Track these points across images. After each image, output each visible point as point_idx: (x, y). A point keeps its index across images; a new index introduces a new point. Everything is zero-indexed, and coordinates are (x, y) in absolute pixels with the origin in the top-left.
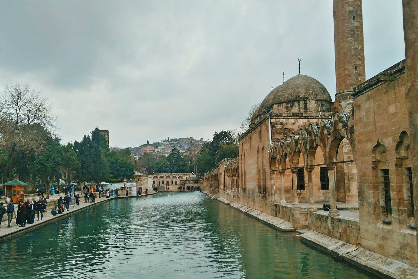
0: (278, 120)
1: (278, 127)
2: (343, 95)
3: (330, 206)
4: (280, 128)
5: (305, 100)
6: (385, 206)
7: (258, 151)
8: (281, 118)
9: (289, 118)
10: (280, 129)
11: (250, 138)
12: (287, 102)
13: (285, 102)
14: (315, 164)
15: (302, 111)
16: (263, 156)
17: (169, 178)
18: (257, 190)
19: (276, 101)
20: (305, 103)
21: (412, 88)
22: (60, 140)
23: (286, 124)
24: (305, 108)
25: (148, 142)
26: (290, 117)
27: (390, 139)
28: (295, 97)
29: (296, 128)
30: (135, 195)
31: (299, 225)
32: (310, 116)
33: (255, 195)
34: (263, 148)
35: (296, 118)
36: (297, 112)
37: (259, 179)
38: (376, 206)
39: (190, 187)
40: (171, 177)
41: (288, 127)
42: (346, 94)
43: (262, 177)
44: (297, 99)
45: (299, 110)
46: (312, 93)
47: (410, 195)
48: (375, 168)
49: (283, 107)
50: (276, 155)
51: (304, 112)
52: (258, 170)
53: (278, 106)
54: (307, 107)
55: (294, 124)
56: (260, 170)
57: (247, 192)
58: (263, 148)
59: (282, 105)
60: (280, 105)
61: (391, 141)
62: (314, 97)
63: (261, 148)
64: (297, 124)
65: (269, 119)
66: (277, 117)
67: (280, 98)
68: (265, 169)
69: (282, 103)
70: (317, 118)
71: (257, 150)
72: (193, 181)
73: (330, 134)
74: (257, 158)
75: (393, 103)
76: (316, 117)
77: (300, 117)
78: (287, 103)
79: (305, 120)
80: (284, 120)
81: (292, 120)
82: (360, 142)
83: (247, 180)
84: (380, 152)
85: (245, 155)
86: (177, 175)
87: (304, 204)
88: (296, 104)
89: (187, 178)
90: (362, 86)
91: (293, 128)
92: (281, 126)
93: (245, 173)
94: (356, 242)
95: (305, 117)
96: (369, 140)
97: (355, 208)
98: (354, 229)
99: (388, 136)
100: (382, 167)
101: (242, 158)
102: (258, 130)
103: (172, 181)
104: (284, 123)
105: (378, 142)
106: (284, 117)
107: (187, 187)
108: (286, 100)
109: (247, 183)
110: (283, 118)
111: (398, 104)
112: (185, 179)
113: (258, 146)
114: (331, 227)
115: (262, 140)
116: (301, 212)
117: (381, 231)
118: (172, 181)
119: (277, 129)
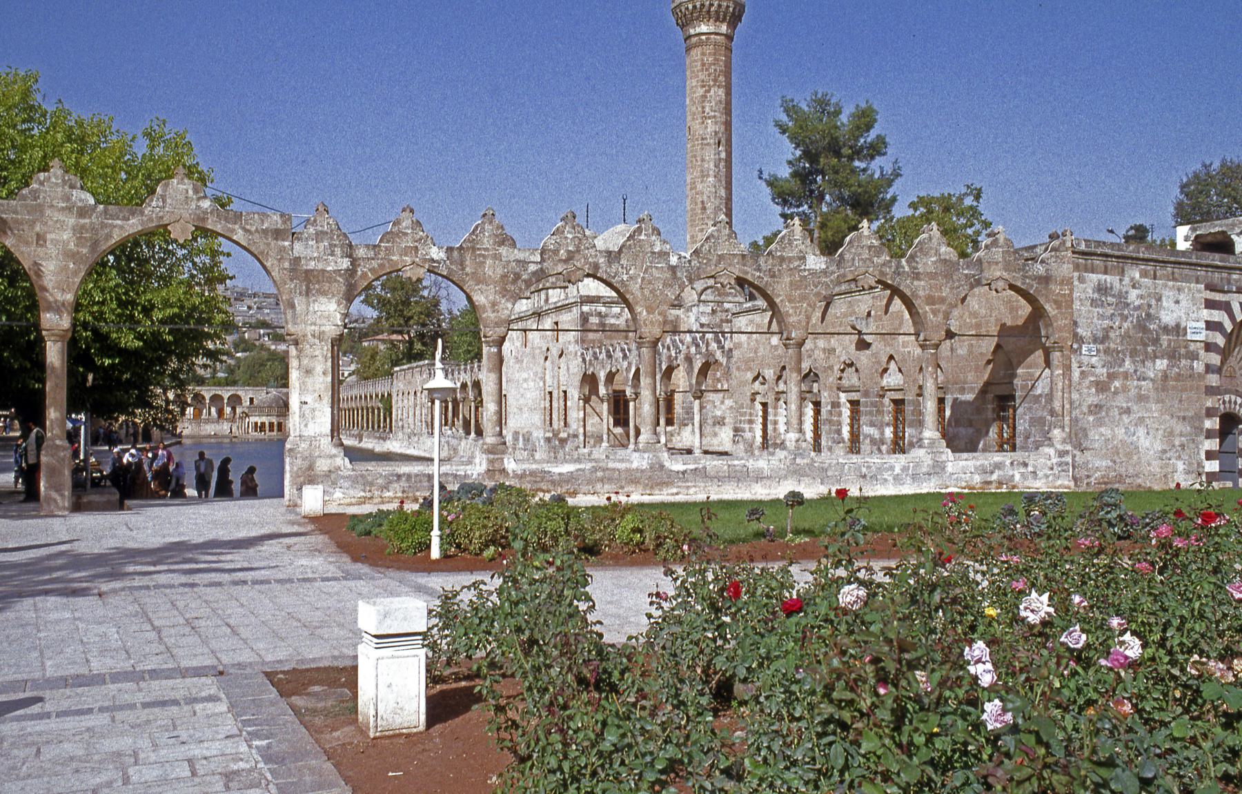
1: (594, 320)
23: (606, 315)
63: (555, 352)
73: (700, 353)
80: (603, 309)
89: (251, 400)
96: (750, 369)
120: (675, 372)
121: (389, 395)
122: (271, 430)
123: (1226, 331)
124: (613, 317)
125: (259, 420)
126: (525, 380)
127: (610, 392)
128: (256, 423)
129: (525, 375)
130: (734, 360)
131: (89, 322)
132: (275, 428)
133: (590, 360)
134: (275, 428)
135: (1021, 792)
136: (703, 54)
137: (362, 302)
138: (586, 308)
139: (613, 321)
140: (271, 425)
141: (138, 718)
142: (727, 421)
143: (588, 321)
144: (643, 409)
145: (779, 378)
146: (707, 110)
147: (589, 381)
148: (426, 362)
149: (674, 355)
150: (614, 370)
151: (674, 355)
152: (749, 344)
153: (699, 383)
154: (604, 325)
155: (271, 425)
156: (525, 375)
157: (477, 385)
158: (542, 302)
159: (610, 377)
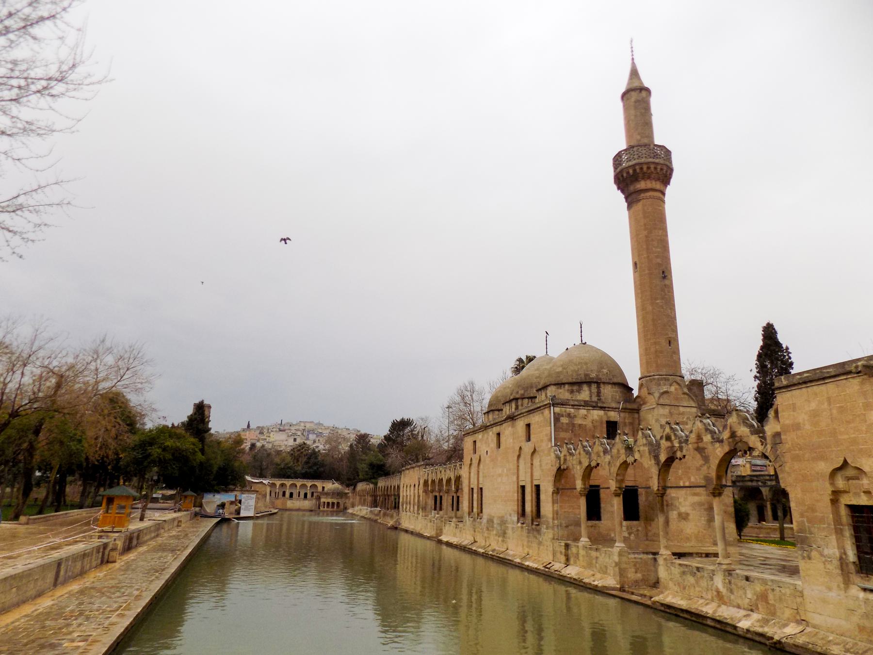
0: (563, 409)
1: (564, 420)
2: (654, 379)
5: (598, 384)
6: (858, 563)
8: (568, 407)
9: (579, 407)
12: (571, 384)
14: (669, 485)
15: (595, 399)
17: (294, 487)
18: (515, 519)
19: (553, 380)
20: (598, 387)
22: (144, 415)
23: (575, 416)
24: (599, 394)
26: (581, 406)
28: (583, 376)
29: (588, 423)
30: (253, 515)
31: (626, 579)
32: (608, 408)
33: (507, 527)
35: (589, 408)
36: (587, 399)
38: (842, 561)
39: (328, 503)
40: (298, 486)
41: (578, 421)
42: (658, 379)
44: (586, 379)
45: (591, 397)
46: (607, 373)
48: (834, 501)
49: (565, 390)
50: (573, 465)
51: (598, 399)
52: (518, 487)
53: (558, 388)
54: (600, 393)
55: (585, 417)
57: (484, 521)
59: (564, 387)
60: (561, 386)
62: (611, 379)
64: (590, 418)
65: (552, 408)
66: (562, 405)
67: (559, 377)
69: (564, 384)
70: (617, 410)
72: (333, 493)
74: (516, 467)
76: (616, 408)
77: (594, 407)
78: (559, 386)
79: (601, 413)
80: (572, 410)
81: (583, 412)
84: (847, 477)
86: (309, 483)
87: (711, 552)
88: (585, 388)
89: (323, 488)
90: (798, 377)
91: (584, 423)
94: (795, 617)
95: (602, 408)
97: (701, 553)
98: (788, 595)
100: (851, 501)
103: (299, 492)
104: (572, 415)
106: (572, 405)
107: (324, 502)
108: (570, 380)
110: (570, 407)
112: (320, 489)
114: (724, 587)
116: (629, 559)
117: (862, 604)
118: (299, 492)
119: (562, 423)
121: (399, 487)
122: (333, 507)
125: (326, 500)
126: (500, 475)
127: (587, 486)
129: (500, 471)
131: (80, 474)
135: (115, 654)
138: (557, 410)
140: (333, 503)
142: (691, 517)
144: (447, 501)
147: (561, 473)
149: (677, 445)
150: (593, 464)
151: (677, 445)
153: (719, 477)
154: (573, 425)
156: (500, 471)
157: (458, 479)
158: (513, 410)
159: (589, 471)
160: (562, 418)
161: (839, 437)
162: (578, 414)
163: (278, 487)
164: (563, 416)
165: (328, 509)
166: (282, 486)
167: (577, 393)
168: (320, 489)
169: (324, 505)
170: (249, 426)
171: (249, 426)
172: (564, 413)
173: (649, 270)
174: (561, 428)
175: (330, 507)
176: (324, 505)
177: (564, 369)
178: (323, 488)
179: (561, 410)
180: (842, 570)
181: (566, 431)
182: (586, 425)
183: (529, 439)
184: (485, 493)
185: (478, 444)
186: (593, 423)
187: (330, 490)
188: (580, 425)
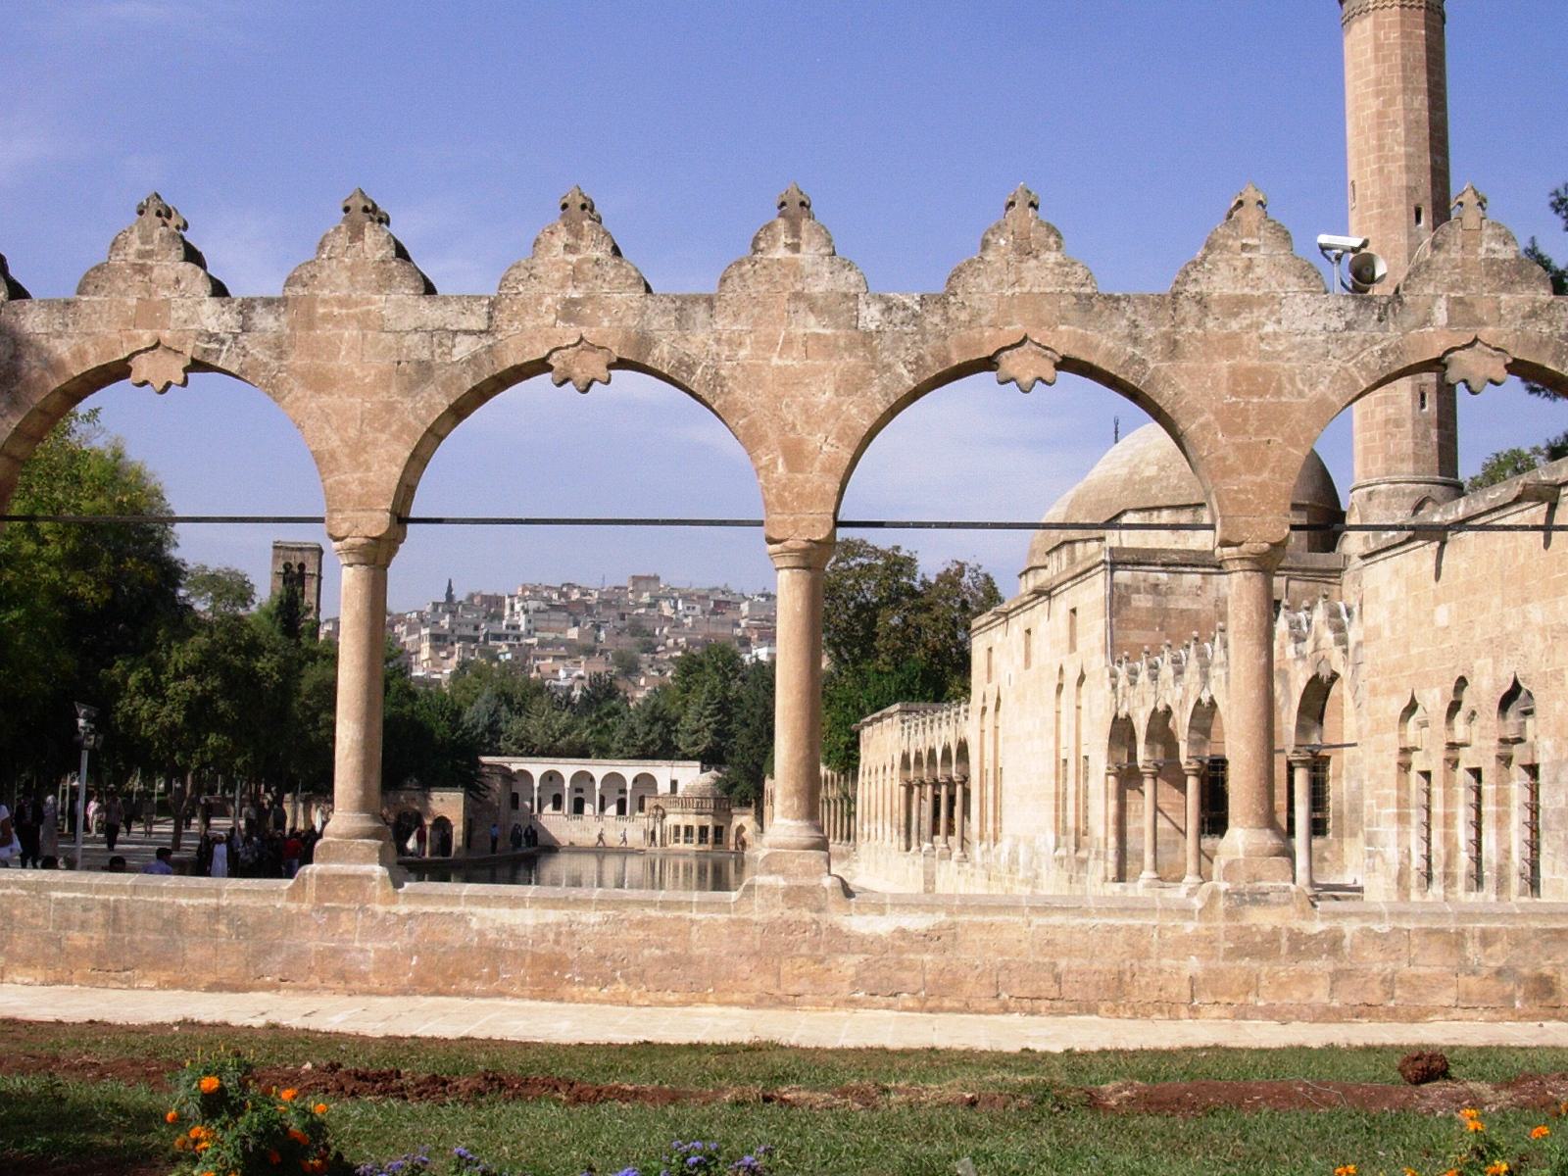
0: (1141, 575)
1: (1142, 601)
3: (1121, 732)
4: (1150, 605)
7: (1060, 687)
9: (1181, 569)
10: (1148, 609)
11: (1028, 632)
13: (1168, 507)
16: (1079, 708)
21: (461, 1082)
23: (1170, 591)
25: (450, 589)
27: (1437, 692)
34: (1082, 679)
35: (1207, 570)
37: (1060, 799)
39: (688, 829)
43: (1071, 788)
47: (1474, 837)
48: (1405, 767)
56: (1086, 758)
58: (1082, 679)
61: (1438, 698)
63: (1072, 676)
68: (1086, 758)
71: (1057, 681)
73: (1304, 658)
75: (1445, 602)
80: (1164, 577)
82: (1374, 691)
83: (1008, 800)
85: (999, 699)
89: (674, 784)
91: (1195, 607)
92: (1150, 597)
93: (998, 772)
96: (1393, 690)
99: (1432, 686)
101: (984, 709)
102: (1061, 605)
104: (1163, 588)
105: (1413, 699)
109: (1006, 813)
111: (1453, 604)
113: (1061, 670)
115: (1080, 647)
119: (1137, 609)
120: (1334, 691)
123: (1281, 828)
124: (1186, 594)
128: (677, 828)
130: (1365, 669)
132: (710, 836)
133: (1124, 687)
134: (710, 836)
136: (1377, 26)
137: (1001, 601)
139: (1183, 603)
141: (1311, 995)
143: (1128, 602)
145: (1454, 707)
146: (1388, 141)
148: (188, 791)
152: (1393, 629)
154: (1166, 613)
155: (703, 830)
160: (1135, 596)
161: (457, 646)
162: (1180, 585)
163: (536, 784)
164: (1138, 591)
165: (689, 846)
166: (551, 779)
167: (262, 640)
168: (664, 787)
169: (677, 833)
170: (450, 596)
171: (450, 596)
172: (1142, 585)
173: (1381, 206)
174: (1133, 620)
175: (696, 838)
176: (677, 833)
177: (1162, 468)
178: (674, 784)
179: (1135, 578)
180: (1399, 884)
181: (1143, 626)
182: (1197, 612)
183: (1073, 647)
184: (1008, 781)
185: (995, 654)
186: (1216, 606)
187: (692, 789)
188: (1182, 611)
